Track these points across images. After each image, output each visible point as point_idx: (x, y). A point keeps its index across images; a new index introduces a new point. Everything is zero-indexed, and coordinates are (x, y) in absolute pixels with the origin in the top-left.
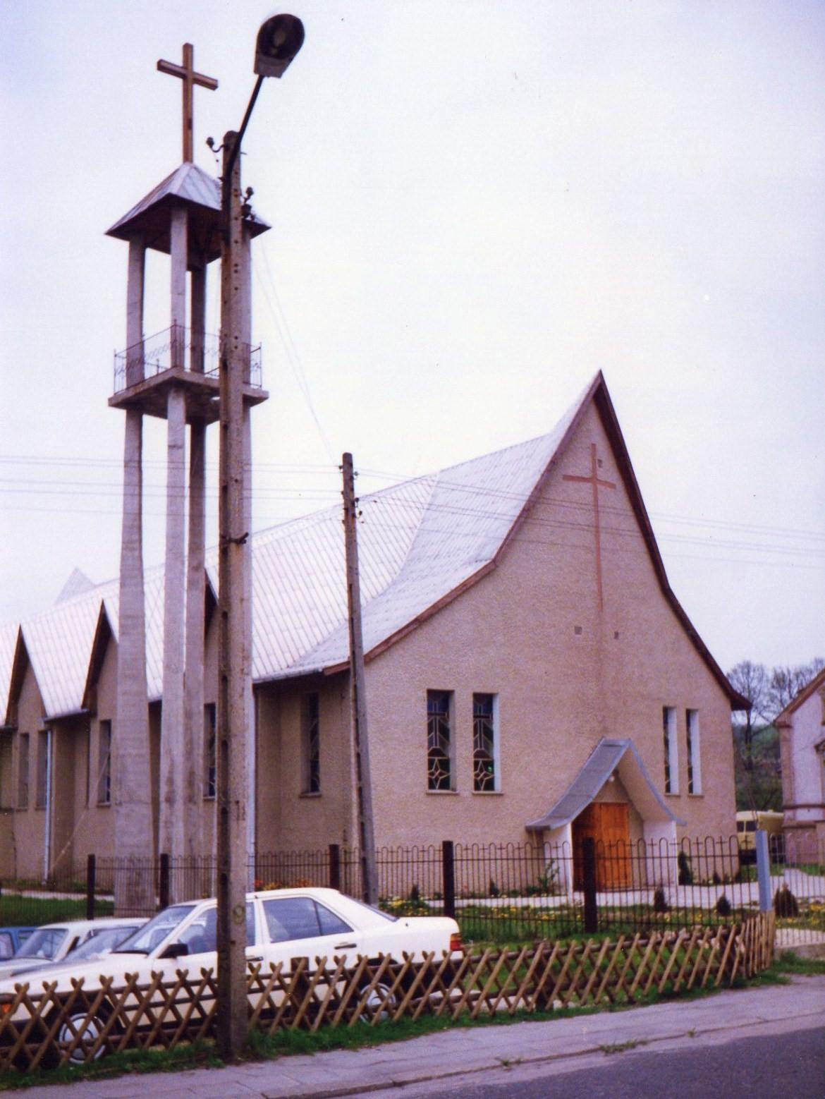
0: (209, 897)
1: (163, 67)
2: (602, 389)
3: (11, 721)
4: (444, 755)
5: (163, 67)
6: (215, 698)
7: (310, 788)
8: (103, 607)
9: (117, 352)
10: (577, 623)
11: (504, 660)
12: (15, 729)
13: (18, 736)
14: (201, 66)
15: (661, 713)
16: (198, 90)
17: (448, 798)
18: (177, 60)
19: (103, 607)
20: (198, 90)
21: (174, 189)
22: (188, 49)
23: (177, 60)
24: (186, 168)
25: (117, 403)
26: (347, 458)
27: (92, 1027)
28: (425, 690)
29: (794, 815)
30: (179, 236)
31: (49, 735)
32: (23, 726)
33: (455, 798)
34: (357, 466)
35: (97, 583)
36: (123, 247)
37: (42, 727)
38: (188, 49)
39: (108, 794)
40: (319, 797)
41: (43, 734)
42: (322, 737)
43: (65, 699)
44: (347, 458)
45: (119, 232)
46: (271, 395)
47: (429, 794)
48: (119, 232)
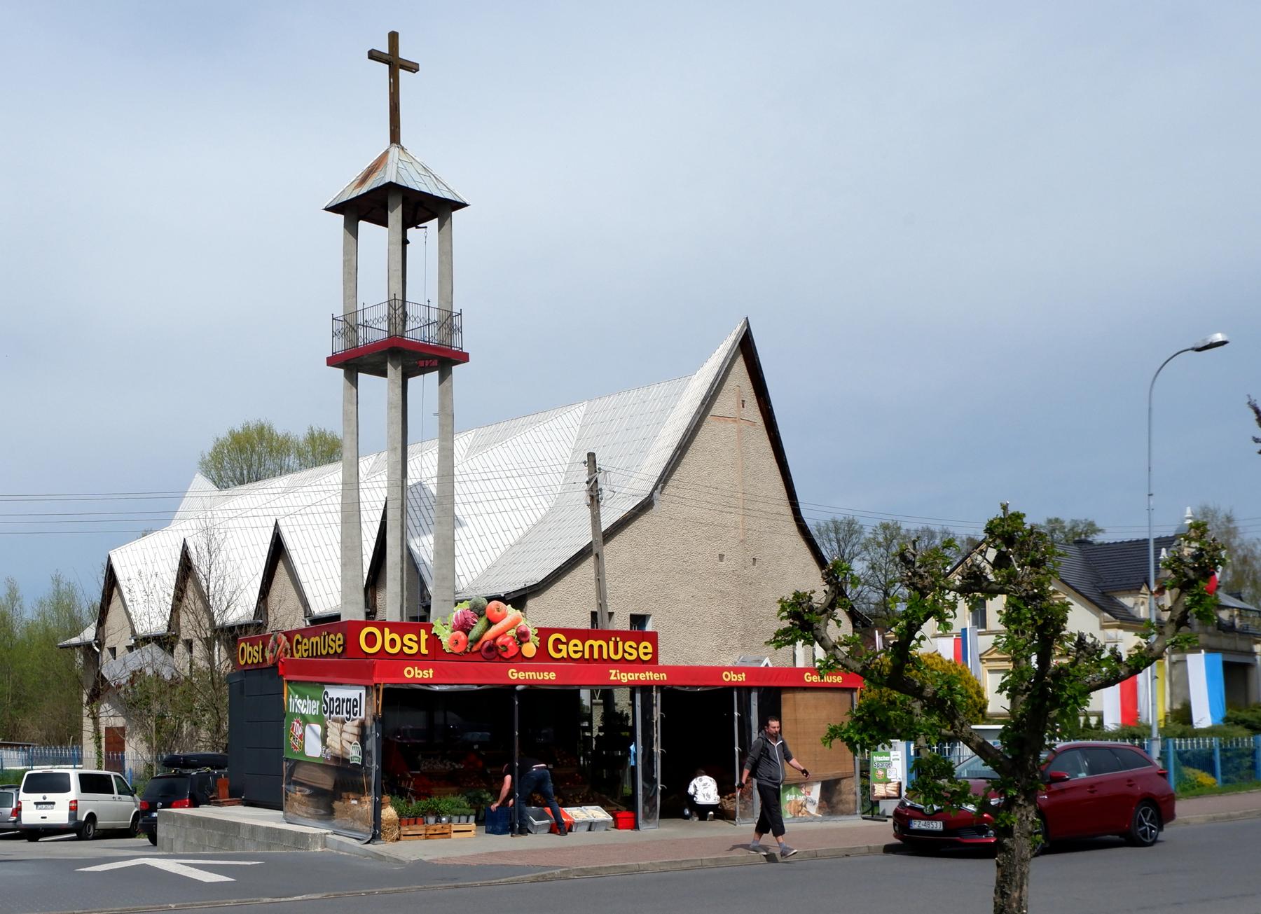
1: (374, 55)
3: (173, 626)
5: (374, 55)
6: (101, 823)
8: (185, 545)
10: (720, 551)
12: (177, 637)
14: (404, 53)
16: (403, 73)
18: (384, 48)
19: (185, 545)
20: (403, 73)
21: (389, 175)
22: (393, 37)
23: (384, 48)
24: (395, 151)
26: (591, 456)
27: (451, 715)
30: (395, 216)
34: (600, 462)
36: (340, 219)
38: (393, 37)
44: (591, 456)
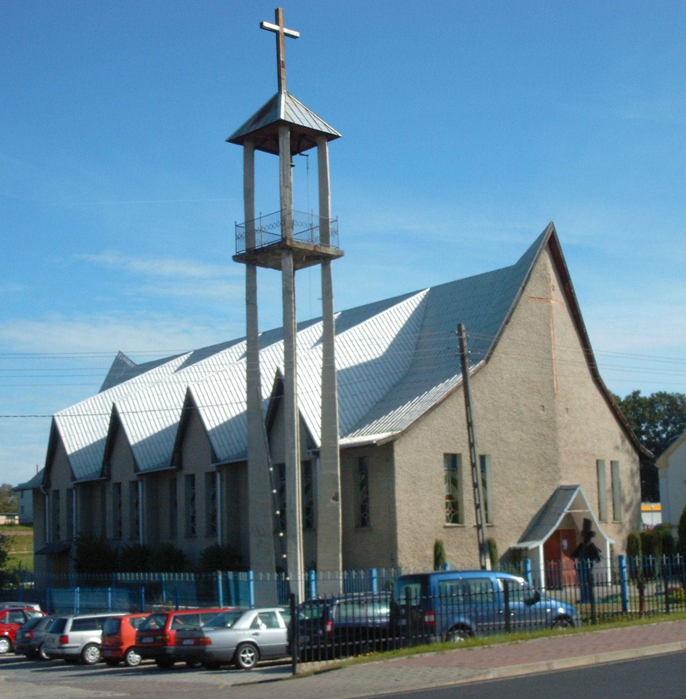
0: (288, 604)
2: (554, 238)
4: (138, 475)
7: (361, 523)
9: (237, 224)
10: (540, 403)
11: (493, 431)
13: (111, 486)
15: (595, 464)
17: (459, 529)
25: (238, 258)
28: (442, 454)
29: (535, 606)
31: (140, 484)
32: (116, 477)
33: (462, 528)
35: (139, 361)
36: (239, 149)
37: (134, 477)
39: (120, 533)
40: (463, 527)
41: (134, 484)
42: (372, 487)
43: (151, 458)
45: (236, 140)
46: (346, 254)
47: (613, 523)
48: (236, 140)
